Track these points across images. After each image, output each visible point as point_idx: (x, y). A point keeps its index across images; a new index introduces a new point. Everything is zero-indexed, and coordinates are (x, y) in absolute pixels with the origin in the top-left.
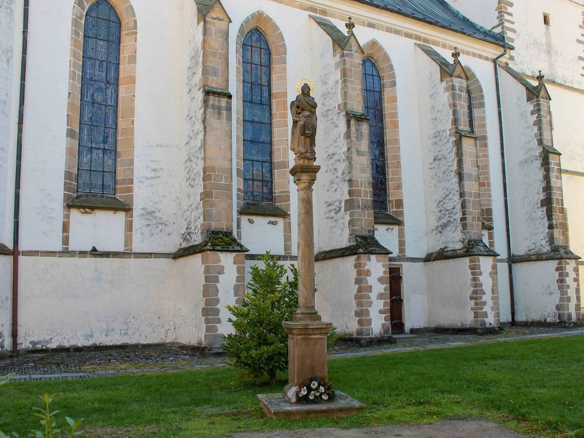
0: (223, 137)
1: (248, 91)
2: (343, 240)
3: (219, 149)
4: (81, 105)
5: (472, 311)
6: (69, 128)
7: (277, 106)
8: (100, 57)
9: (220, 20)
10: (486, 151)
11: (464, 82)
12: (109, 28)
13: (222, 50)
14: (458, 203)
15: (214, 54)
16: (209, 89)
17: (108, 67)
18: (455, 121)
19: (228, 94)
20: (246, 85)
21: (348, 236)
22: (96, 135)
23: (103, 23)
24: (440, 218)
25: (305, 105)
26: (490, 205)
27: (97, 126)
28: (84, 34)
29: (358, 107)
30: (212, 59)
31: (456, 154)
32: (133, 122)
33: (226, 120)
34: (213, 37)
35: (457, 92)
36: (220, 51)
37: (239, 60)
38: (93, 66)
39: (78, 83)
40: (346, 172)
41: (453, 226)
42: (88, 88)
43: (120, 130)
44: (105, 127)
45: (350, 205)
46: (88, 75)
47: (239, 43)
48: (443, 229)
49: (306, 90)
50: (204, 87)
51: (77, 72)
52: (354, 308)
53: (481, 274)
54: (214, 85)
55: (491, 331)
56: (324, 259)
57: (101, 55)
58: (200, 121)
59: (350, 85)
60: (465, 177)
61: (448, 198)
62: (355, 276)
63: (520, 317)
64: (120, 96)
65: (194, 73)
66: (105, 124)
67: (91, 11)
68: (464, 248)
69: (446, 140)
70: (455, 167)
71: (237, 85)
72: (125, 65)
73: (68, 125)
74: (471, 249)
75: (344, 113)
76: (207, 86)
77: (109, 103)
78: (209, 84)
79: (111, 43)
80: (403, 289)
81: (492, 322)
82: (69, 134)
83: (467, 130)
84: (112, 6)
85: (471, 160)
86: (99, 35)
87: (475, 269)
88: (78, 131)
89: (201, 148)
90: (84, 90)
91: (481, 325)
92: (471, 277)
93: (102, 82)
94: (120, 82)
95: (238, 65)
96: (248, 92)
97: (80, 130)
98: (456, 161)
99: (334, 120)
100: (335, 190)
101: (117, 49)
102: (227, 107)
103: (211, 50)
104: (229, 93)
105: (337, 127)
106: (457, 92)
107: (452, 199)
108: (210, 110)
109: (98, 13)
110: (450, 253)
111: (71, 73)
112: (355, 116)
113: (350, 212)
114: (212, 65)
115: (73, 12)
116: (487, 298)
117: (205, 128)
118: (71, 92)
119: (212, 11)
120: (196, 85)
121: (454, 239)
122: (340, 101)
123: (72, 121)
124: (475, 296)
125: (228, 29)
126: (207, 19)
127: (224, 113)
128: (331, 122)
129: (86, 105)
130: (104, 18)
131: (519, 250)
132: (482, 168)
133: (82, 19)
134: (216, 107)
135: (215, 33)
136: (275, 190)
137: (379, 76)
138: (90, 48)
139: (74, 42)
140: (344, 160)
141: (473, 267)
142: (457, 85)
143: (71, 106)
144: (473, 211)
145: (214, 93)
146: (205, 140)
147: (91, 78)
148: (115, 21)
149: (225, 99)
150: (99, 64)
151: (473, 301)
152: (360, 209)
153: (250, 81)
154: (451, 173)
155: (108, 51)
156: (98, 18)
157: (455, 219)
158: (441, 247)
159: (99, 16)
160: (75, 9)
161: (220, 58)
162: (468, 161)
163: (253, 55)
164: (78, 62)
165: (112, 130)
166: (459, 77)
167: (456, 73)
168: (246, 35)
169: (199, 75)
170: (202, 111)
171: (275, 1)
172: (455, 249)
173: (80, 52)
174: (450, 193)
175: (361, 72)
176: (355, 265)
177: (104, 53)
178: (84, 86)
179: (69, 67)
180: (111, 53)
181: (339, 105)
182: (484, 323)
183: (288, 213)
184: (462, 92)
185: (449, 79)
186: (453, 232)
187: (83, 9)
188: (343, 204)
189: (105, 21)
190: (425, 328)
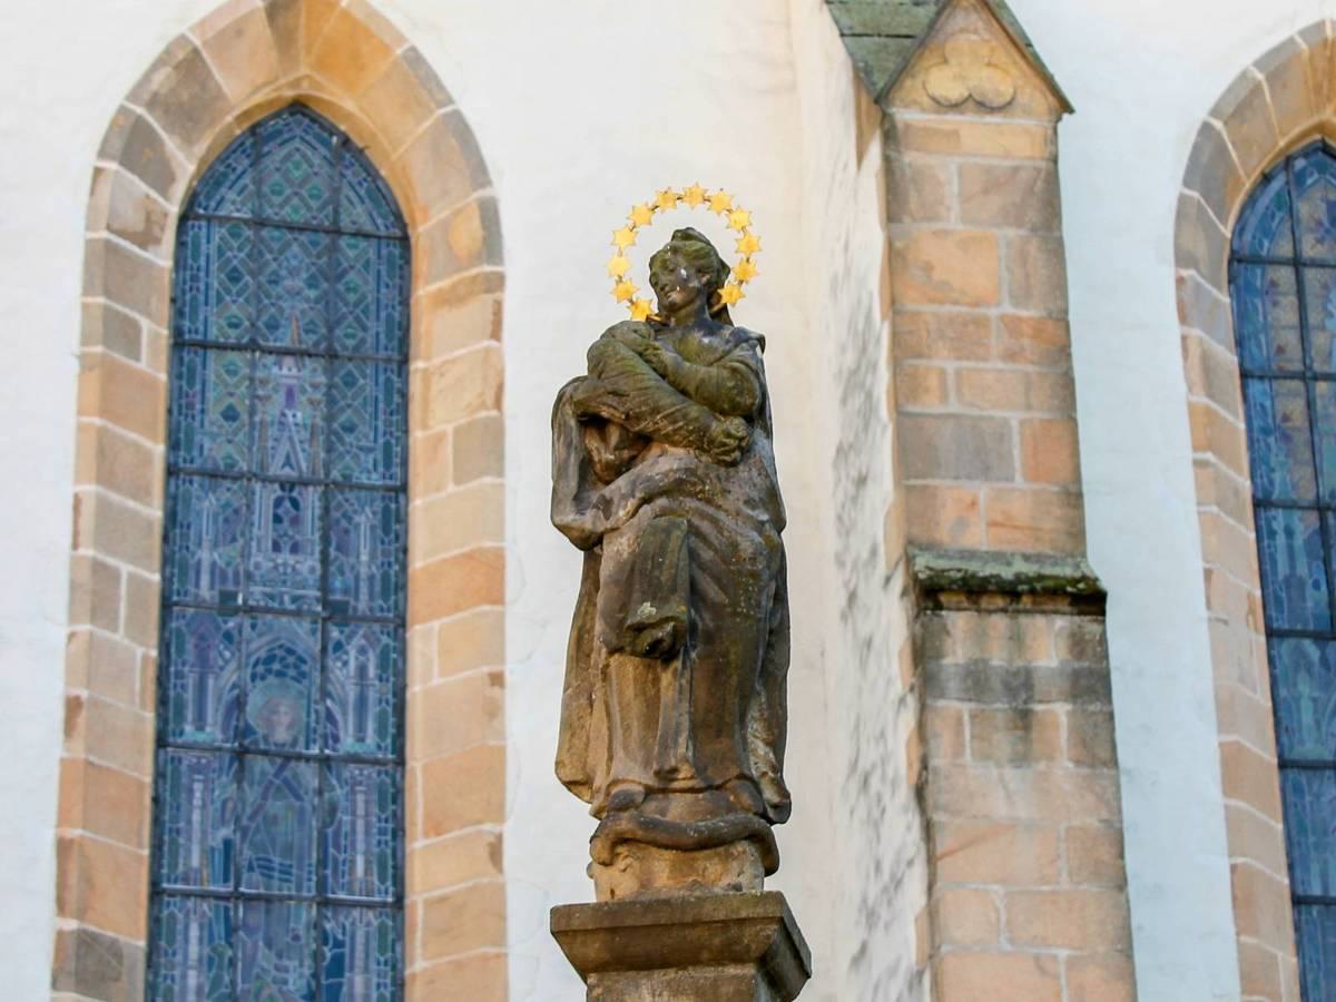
0: (1065, 884)
3: (1042, 970)
4: (159, 775)
6: (71, 925)
8: (280, 459)
9: (992, 110)
12: (334, 274)
13: (1022, 296)
15: (967, 336)
16: (941, 564)
17: (335, 515)
19: (1075, 582)
20: (1278, 526)
22: (265, 958)
23: (295, 248)
25: (672, 404)
27: (268, 900)
28: (177, 333)
30: (951, 366)
32: (495, 852)
33: (1078, 762)
34: (953, 220)
36: (1008, 308)
37: (1208, 366)
38: (233, 524)
39: (135, 633)
42: (203, 662)
43: (420, 912)
44: (324, 903)
46: (205, 580)
47: (1201, 249)
49: (693, 282)
50: (909, 560)
51: (125, 569)
54: (978, 537)
57: (284, 448)
58: (905, 793)
64: (415, 691)
65: (862, 481)
66: (322, 885)
67: (218, 184)
71: (1208, 525)
72: (438, 489)
73: (62, 907)
76: (930, 547)
77: (348, 744)
78: (944, 535)
79: (350, 366)
82: (71, 965)
84: (346, 142)
86: (273, 326)
88: (142, 943)
89: (920, 974)
90: (179, 675)
93: (298, 614)
94: (418, 600)
95: (1201, 399)
96: (1302, 569)
97: (153, 938)
101: (388, 402)
102: (1076, 676)
103: (948, 309)
104: (1084, 578)
108: (953, 706)
109: (259, 194)
111: (85, 575)
114: (954, 407)
115: (92, 210)
117: (928, 830)
118: (84, 694)
119: (930, 58)
120: (874, 552)
123: (88, 881)
125: (1055, 160)
126: (903, 115)
127: (1058, 714)
129: (194, 769)
130: (300, 217)
133: (157, 241)
134: (996, 684)
135: (965, 199)
138: (214, 414)
139: (106, 385)
143: (83, 785)
145: (975, 590)
146: (932, 913)
147: (227, 597)
148: (369, 228)
149: (1061, 622)
150: (278, 502)
153: (1310, 496)
155: (329, 418)
156: (260, 223)
159: (269, 212)
160: (105, 189)
161: (1011, 356)
163: (1314, 318)
164: (131, 504)
165: (371, 915)
168: (1252, 200)
169: (883, 489)
170: (908, 718)
173: (147, 443)
177: (305, 435)
178: (181, 651)
179: (67, 540)
180: (350, 429)
187: (161, 177)
189: (304, 238)
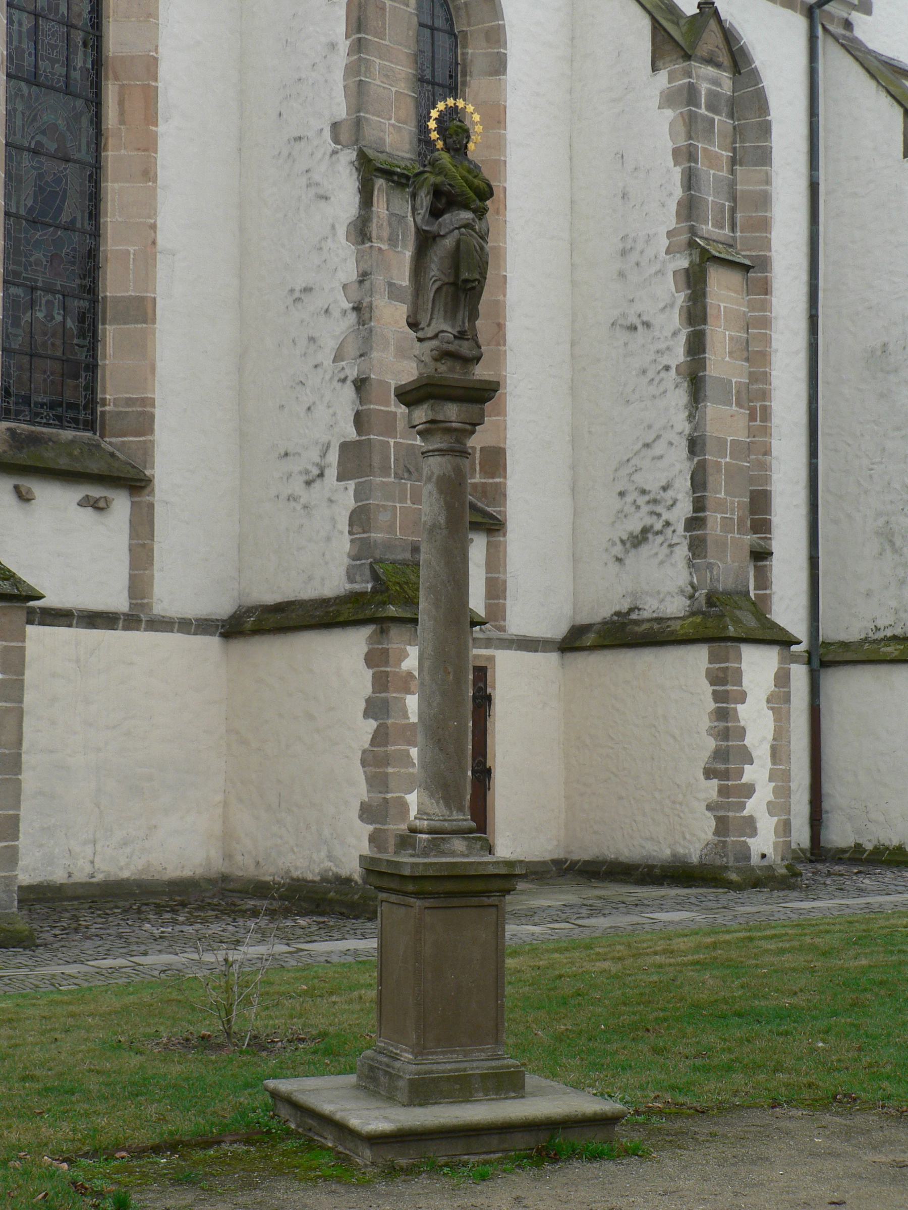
1: (25, 40)
2: (328, 571)
5: (708, 814)
7: (121, 103)
10: (765, 306)
11: (725, 77)
14: (681, 472)
18: (690, 208)
21: (346, 561)
24: (622, 515)
26: (767, 479)
29: (395, 138)
31: (685, 315)
35: (703, 111)
40: (352, 350)
41: (662, 544)
45: (355, 459)
48: (627, 552)
52: (360, 791)
53: (742, 698)
55: (761, 880)
56: (258, 631)
59: (378, 61)
60: (710, 389)
61: (650, 453)
62: (367, 689)
63: (839, 834)
68: (693, 614)
69: (653, 270)
70: (679, 355)
74: (723, 622)
75: (353, 156)
80: (494, 737)
81: (769, 850)
83: (722, 239)
85: (731, 338)
87: (725, 687)
91: (737, 860)
92: (711, 705)
98: (682, 338)
99: (317, 177)
100: (309, 409)
105: (326, 198)
106: (703, 111)
107: (661, 457)
110: (645, 626)
112: (387, 174)
113: (357, 485)
116: (758, 774)
121: (663, 584)
122: (341, 111)
124: (723, 767)
128: (304, 181)
131: (844, 625)
132: (755, 355)
136: (104, 392)
137: (452, 33)
140: (344, 312)
141: (721, 675)
142: (704, 87)
144: (726, 501)
151: (715, 782)
152: (389, 476)
154: (663, 374)
157: (668, 524)
158: (617, 608)
162: (721, 337)
166: (710, 61)
167: (703, 49)
171: (905, 136)
172: (661, 615)
174: (658, 437)
175: (415, 20)
176: (367, 654)
181: (335, 126)
182: (744, 854)
183: (147, 472)
184: (717, 113)
185: (680, 66)
186: (662, 563)
188: (333, 457)
190: (557, 862)
